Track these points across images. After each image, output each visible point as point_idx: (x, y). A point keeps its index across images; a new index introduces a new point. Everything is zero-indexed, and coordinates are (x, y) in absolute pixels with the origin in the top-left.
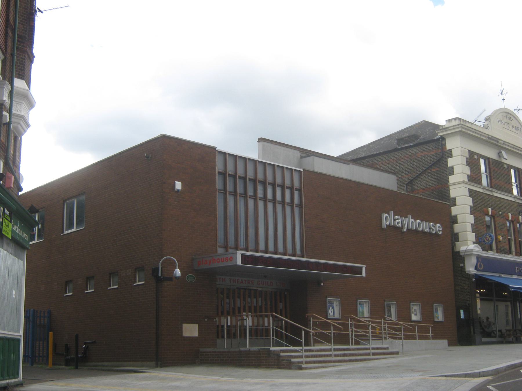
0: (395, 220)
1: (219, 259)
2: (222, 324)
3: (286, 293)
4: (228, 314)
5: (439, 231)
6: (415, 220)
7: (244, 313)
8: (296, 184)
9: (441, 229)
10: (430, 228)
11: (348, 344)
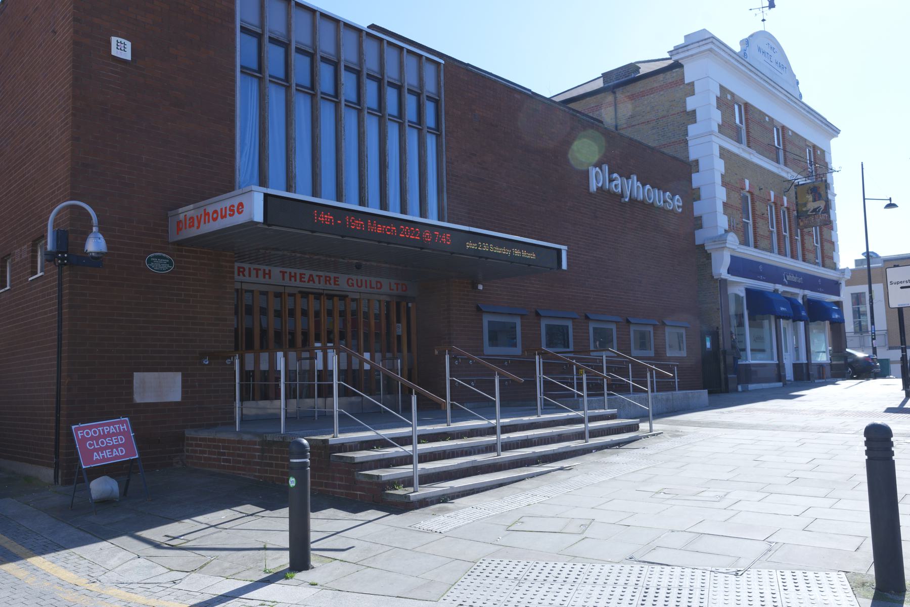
0: (611, 180)
1: (215, 212)
2: (330, 368)
3: (410, 305)
4: (279, 346)
5: (679, 207)
6: (644, 185)
7: (318, 345)
8: (430, 87)
9: (681, 204)
10: (665, 202)
11: (534, 412)
